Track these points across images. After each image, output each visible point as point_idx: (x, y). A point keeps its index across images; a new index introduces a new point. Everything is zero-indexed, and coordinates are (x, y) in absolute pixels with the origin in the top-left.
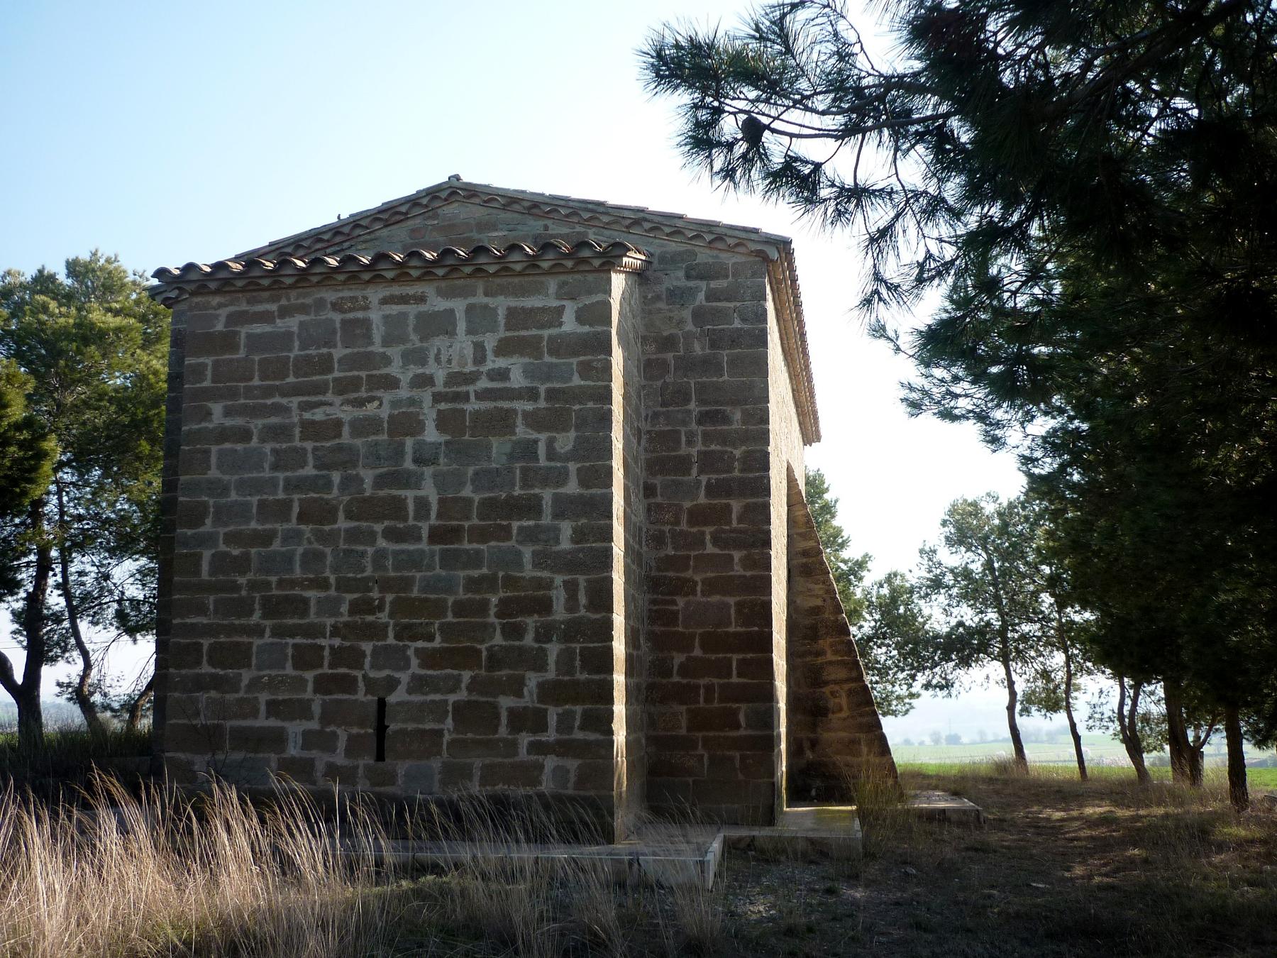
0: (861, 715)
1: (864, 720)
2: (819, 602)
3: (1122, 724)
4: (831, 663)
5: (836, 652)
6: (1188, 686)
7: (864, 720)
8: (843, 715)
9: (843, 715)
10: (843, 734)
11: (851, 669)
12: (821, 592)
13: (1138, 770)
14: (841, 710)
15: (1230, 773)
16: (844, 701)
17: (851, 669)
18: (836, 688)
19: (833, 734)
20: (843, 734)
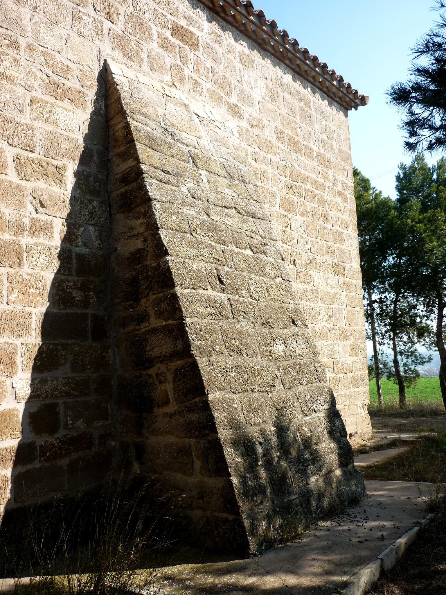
0: (190, 410)
1: (193, 417)
2: (139, 244)
3: (441, 300)
4: (153, 331)
5: (159, 314)
6: (257, 498)
7: (193, 417)
8: (170, 409)
9: (170, 409)
10: (172, 439)
11: (176, 339)
12: (142, 229)
13: (400, 402)
14: (167, 402)
15: (441, 376)
16: (169, 387)
17: (176, 339)
18: (162, 367)
19: (160, 439)
20: (172, 439)
